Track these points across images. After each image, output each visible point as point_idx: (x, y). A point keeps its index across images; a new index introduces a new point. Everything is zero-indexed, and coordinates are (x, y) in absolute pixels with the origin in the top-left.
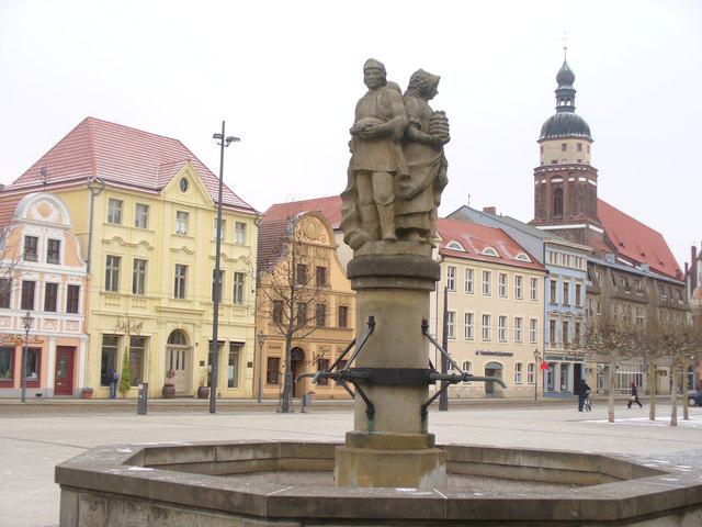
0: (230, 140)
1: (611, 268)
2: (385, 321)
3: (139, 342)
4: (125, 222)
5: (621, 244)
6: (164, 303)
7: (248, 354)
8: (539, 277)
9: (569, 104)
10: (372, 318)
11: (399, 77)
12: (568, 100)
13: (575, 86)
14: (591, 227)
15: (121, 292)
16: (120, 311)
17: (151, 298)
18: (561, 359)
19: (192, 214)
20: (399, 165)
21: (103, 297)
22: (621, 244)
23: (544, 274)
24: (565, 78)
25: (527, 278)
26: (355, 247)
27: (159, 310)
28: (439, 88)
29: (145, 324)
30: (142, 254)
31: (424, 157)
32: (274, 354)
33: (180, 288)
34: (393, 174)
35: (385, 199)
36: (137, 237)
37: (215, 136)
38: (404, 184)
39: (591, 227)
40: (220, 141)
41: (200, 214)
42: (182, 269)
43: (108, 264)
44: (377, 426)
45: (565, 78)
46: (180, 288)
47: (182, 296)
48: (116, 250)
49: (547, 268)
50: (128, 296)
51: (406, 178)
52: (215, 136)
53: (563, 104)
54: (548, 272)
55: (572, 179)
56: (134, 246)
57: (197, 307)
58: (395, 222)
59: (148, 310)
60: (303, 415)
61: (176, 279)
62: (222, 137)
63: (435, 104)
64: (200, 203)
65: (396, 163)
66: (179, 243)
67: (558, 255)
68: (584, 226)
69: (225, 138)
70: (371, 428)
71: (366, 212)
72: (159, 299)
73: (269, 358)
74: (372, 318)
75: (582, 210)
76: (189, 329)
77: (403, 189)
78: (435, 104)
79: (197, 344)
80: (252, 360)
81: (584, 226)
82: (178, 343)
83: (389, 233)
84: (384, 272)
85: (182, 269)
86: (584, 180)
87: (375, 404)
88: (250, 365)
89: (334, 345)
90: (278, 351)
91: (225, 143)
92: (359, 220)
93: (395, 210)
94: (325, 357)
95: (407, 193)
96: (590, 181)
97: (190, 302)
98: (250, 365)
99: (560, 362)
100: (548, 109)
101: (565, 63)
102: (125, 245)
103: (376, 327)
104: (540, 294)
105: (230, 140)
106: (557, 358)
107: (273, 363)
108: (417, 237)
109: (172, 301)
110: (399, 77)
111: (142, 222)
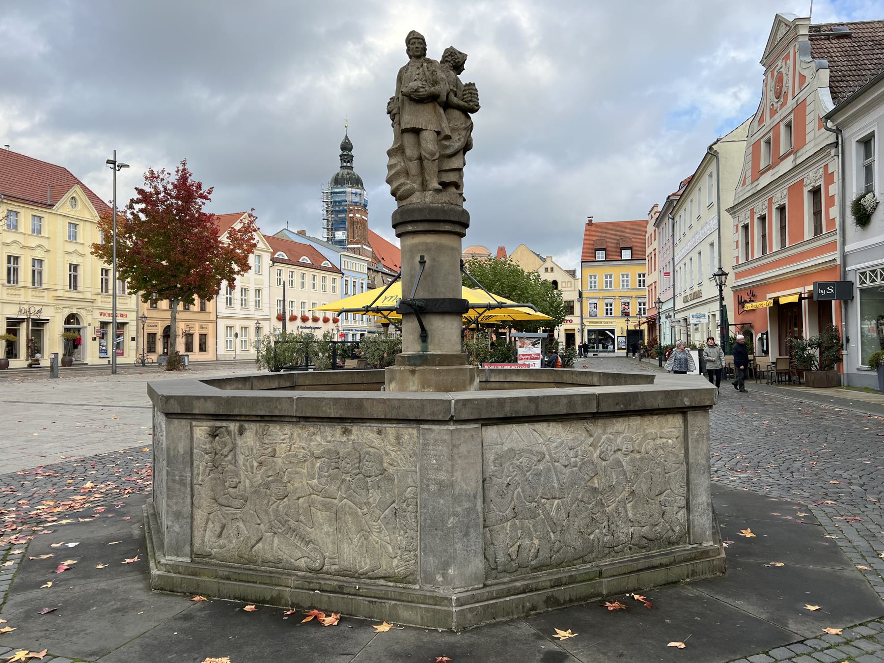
0: (121, 166)
1: (382, 273)
2: (434, 260)
3: (39, 324)
4: (21, 229)
5: (383, 259)
6: (60, 293)
7: (130, 331)
8: (338, 277)
9: (348, 164)
10: (422, 257)
11: (435, 53)
12: (348, 162)
13: (353, 152)
14: (364, 247)
15: (21, 284)
16: (22, 299)
17: (49, 290)
18: (352, 330)
19: (81, 224)
20: (444, 125)
21: (5, 288)
22: (383, 259)
23: (341, 275)
24: (346, 147)
25: (330, 276)
26: (399, 199)
27: (57, 299)
28: (465, 66)
29: (45, 309)
30: (39, 254)
31: (448, 122)
32: (152, 330)
33: (73, 282)
34: (438, 133)
35: (433, 155)
36: (34, 242)
37: (109, 162)
38: (446, 143)
39: (364, 247)
40: (112, 166)
41: (88, 224)
42: (74, 267)
43: (9, 262)
44: (430, 347)
45: (346, 147)
46: (73, 282)
47: (76, 287)
48: (14, 251)
49: (342, 271)
50: (27, 287)
51: (448, 138)
52: (109, 162)
53: (345, 164)
54: (343, 274)
55: (351, 215)
56: (32, 249)
57: (88, 296)
58: (439, 177)
59: (47, 297)
60: (419, 335)
61: (70, 275)
62: (114, 163)
63: (464, 78)
64: (87, 216)
65: (441, 125)
66: (71, 247)
67: (349, 263)
68: (359, 246)
69: (117, 164)
70: (425, 349)
71: (413, 167)
72: (56, 290)
73: (201, 335)
74: (422, 257)
75: (358, 236)
76: (83, 313)
77: (447, 147)
78: (464, 78)
79: (90, 325)
80: (134, 335)
81: (359, 246)
82: (73, 323)
83: (435, 184)
84: (433, 217)
85: (74, 267)
86: (359, 216)
87: (429, 333)
88: (133, 339)
89: (197, 324)
90: (155, 328)
91: (117, 168)
92: (406, 173)
93: (439, 166)
94: (191, 332)
95: (448, 152)
96: (363, 217)
97: (83, 292)
98: (133, 339)
99: (351, 332)
100: (335, 167)
101: (346, 136)
102: (23, 247)
103: (427, 265)
104: (338, 290)
105: (121, 166)
106: (349, 330)
107: (152, 337)
108: (453, 190)
109: (66, 291)
110: (435, 53)
111: (37, 231)
